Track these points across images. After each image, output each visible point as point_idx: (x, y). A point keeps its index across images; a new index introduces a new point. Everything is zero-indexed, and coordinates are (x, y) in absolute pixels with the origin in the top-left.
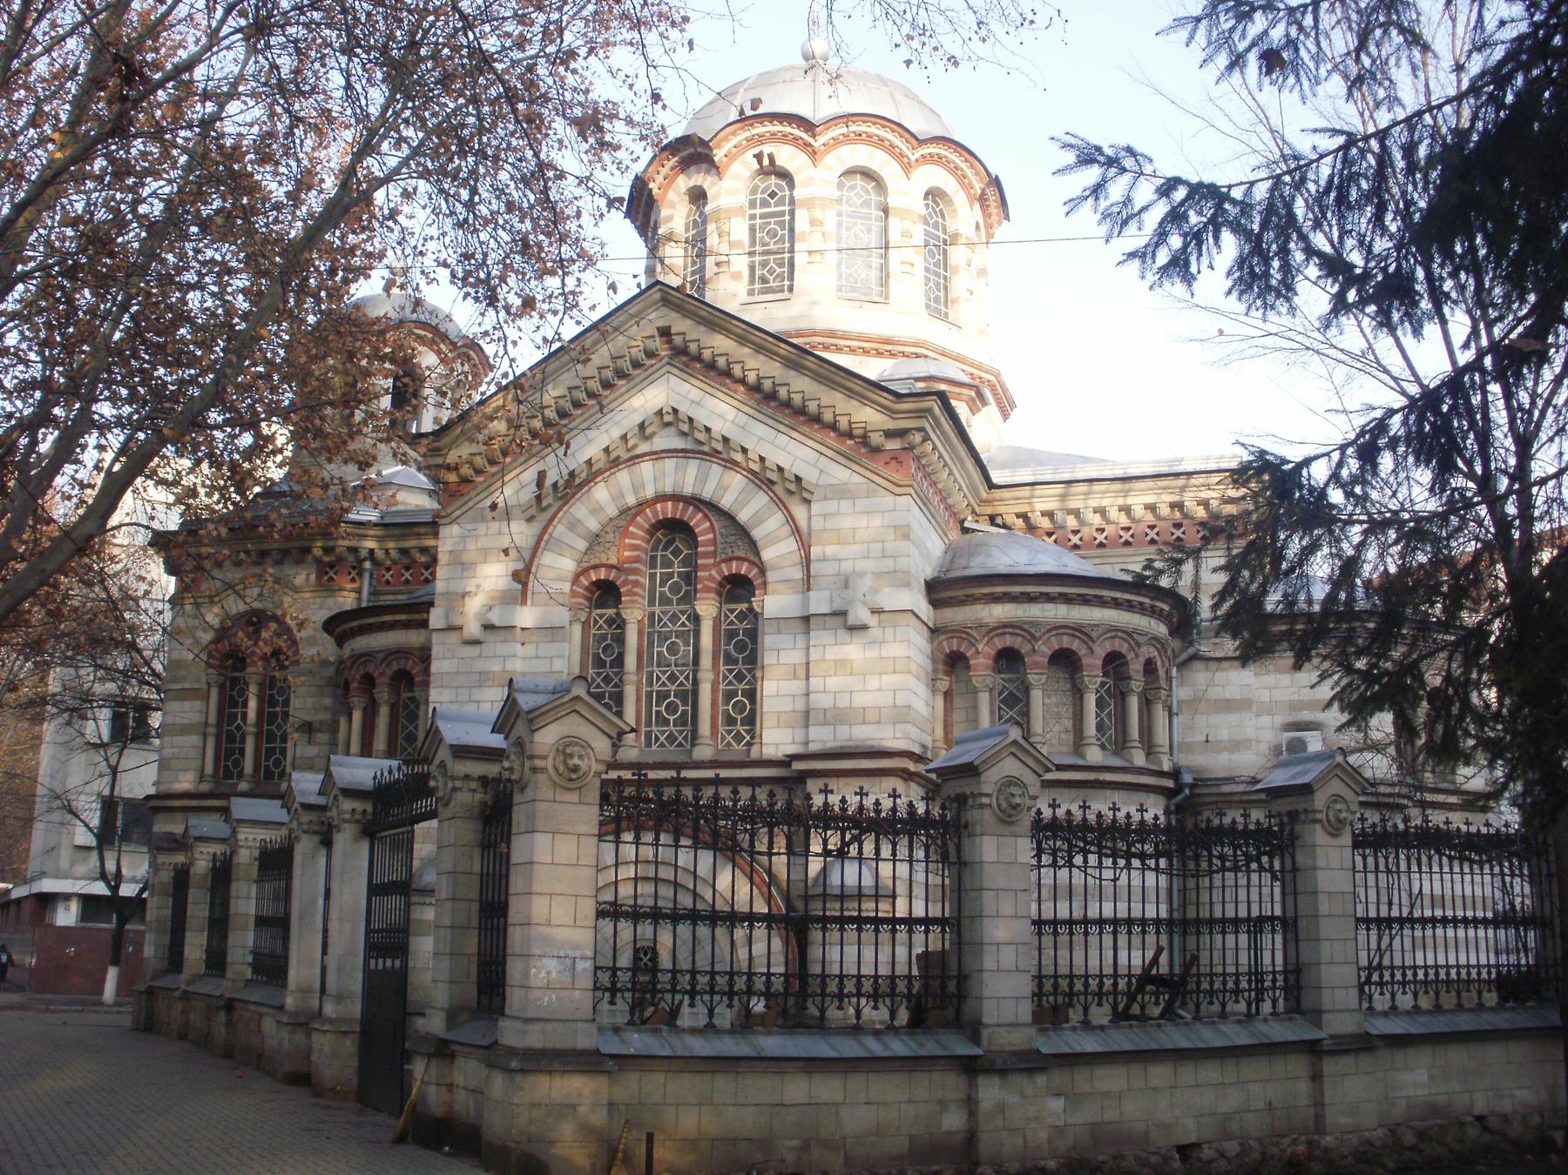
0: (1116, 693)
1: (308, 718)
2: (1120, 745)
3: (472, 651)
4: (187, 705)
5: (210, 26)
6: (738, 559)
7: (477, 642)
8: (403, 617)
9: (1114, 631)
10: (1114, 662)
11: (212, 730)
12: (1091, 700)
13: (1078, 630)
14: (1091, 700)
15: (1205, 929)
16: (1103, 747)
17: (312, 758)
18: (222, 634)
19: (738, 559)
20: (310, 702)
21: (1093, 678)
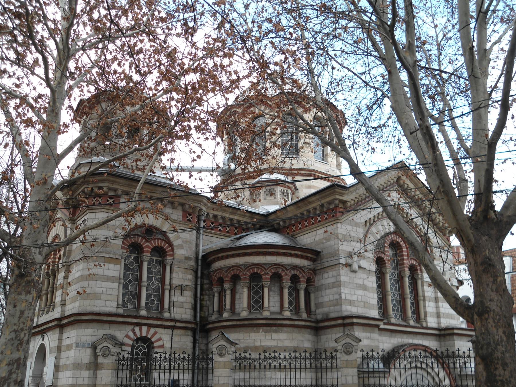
0: (294, 291)
1: (181, 283)
2: (297, 310)
3: (353, 275)
4: (111, 266)
5: (375, 57)
6: (158, 239)
7: (355, 272)
8: (299, 253)
9: (295, 267)
10: (295, 279)
11: (167, 287)
12: (286, 292)
13: (259, 265)
14: (286, 292)
16: (291, 311)
17: (182, 303)
19: (158, 239)
20: (181, 276)
21: (287, 283)
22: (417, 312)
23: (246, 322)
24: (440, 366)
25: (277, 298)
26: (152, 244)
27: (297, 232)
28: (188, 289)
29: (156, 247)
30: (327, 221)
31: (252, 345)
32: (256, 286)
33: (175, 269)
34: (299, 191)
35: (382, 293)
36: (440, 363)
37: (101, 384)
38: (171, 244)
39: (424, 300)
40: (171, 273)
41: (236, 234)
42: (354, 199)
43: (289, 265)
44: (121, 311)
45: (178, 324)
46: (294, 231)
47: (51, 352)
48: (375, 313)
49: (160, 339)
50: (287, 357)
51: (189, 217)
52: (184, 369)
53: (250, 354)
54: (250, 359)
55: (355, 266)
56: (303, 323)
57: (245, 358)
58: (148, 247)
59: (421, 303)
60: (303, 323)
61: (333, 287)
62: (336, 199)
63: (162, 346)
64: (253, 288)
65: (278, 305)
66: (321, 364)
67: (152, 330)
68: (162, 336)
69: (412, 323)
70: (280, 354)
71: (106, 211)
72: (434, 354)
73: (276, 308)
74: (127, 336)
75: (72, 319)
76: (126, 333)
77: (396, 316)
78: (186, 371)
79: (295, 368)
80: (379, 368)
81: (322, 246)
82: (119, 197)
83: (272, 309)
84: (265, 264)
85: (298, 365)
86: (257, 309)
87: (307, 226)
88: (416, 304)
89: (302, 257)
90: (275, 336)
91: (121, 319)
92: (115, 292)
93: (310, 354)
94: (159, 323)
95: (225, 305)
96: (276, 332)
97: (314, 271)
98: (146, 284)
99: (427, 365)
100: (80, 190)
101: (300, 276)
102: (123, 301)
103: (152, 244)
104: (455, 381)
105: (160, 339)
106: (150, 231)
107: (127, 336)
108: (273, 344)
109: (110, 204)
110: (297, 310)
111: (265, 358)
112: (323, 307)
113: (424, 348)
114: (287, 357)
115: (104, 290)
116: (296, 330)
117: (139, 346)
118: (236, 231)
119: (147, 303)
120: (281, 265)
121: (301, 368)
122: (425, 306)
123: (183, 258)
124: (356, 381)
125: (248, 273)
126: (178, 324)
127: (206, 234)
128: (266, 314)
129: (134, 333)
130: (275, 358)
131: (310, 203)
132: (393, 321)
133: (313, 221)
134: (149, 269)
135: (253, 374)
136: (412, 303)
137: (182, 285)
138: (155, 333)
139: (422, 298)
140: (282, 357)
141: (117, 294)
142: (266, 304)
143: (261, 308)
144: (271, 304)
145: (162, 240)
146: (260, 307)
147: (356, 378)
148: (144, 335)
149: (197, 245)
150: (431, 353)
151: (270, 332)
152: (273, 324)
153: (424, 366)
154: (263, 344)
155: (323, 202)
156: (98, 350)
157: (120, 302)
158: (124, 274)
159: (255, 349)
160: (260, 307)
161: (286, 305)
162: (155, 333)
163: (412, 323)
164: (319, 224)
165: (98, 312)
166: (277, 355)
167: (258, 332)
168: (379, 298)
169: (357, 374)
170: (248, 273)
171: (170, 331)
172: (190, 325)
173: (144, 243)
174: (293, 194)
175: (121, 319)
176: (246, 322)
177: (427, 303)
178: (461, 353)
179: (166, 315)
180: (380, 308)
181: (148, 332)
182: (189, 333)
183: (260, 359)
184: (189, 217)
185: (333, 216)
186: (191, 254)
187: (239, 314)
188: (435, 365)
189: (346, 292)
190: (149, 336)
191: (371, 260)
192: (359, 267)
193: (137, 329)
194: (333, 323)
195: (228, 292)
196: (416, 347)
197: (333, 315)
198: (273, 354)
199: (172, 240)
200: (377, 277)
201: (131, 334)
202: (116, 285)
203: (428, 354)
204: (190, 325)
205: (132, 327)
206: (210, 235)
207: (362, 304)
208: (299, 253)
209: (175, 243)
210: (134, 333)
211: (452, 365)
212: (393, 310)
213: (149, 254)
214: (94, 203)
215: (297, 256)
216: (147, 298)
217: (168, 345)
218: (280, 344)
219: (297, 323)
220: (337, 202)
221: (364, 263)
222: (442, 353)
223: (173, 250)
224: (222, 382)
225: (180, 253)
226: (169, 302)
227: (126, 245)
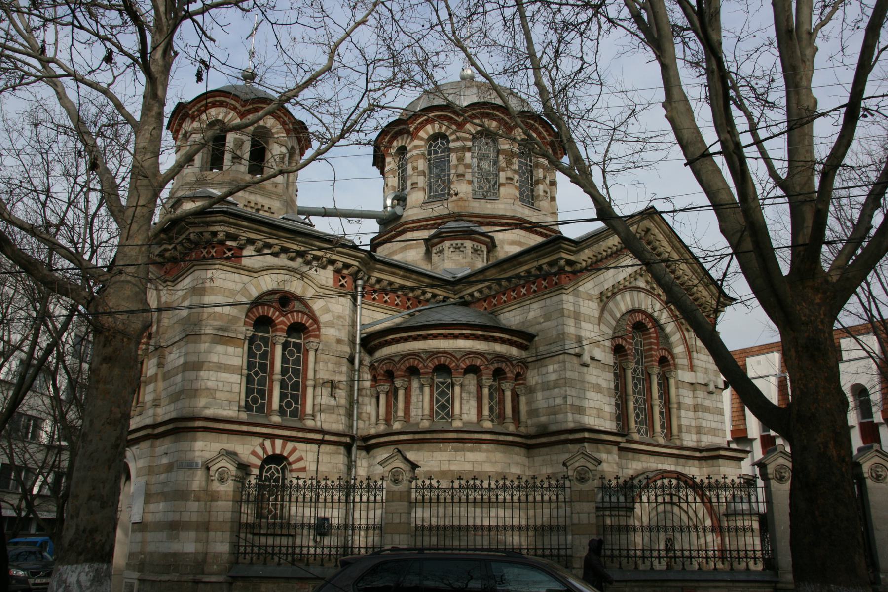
1: (331, 378)
6: (298, 312)
9: (499, 357)
13: (414, 354)
15: (741, 533)
18: (257, 302)
19: (298, 312)
22: (667, 426)
23: (428, 436)
24: (698, 500)
25: (474, 403)
26: (288, 319)
27: (499, 307)
28: (341, 386)
29: (295, 323)
30: (547, 291)
31: (436, 469)
32: (443, 383)
33: (321, 356)
34: (499, 248)
35: (620, 396)
36: (699, 495)
37: (216, 522)
38: (315, 320)
39: (679, 409)
40: (315, 362)
41: (408, 308)
42: (586, 259)
43: (490, 354)
44: (244, 416)
45: (327, 437)
46: (495, 305)
47: (138, 476)
48: (609, 425)
49: (300, 459)
50: (493, 486)
51: (343, 282)
52: (297, 501)
53: (438, 482)
54: (438, 488)
55: (586, 358)
56: (510, 438)
57: (431, 487)
58: (283, 322)
59: (674, 411)
60: (510, 438)
61: (554, 388)
62: (562, 258)
63: (304, 469)
64: (438, 387)
65: (474, 411)
66: (542, 496)
67: (290, 445)
68: (304, 455)
69: (661, 440)
70: (482, 482)
71: (220, 267)
72: (690, 482)
73: (474, 418)
74: (254, 453)
75: (170, 426)
76: (251, 449)
77: (639, 431)
78: (539, 505)
79: (460, 502)
80: (618, 502)
81: (538, 327)
82: (241, 248)
83: (465, 417)
84: (456, 352)
85: (464, 498)
86: (443, 418)
87: (515, 298)
88: (667, 414)
89: (511, 343)
90: (470, 456)
91: (244, 428)
92: (236, 388)
93: (512, 481)
94: (300, 434)
95: (396, 412)
96: (471, 450)
97: (524, 364)
98: (280, 377)
99: (680, 498)
100: (183, 236)
101: (507, 370)
102: (247, 401)
103: (288, 319)
104: (719, 521)
105: (300, 459)
106: (285, 299)
107: (254, 453)
108: (468, 467)
109: (228, 258)
110: (501, 417)
111: (461, 487)
112: (538, 416)
113: (675, 475)
114: (493, 486)
115: (220, 385)
116: (501, 447)
117: (271, 468)
118: (409, 304)
119: (281, 406)
120: (445, 352)
121: (453, 502)
122: (679, 417)
123: (335, 340)
124: (593, 520)
125: (430, 364)
126: (327, 437)
127: (366, 307)
128: (457, 424)
129: (264, 449)
130: (475, 488)
131: (521, 264)
132: (636, 437)
133: (524, 291)
134: (283, 355)
135: (539, 511)
136: (661, 413)
137: (332, 382)
138: (294, 450)
139: (675, 406)
140: (486, 485)
141: (238, 391)
142: (457, 410)
143: (451, 416)
144: (464, 411)
145: (304, 313)
146: (447, 415)
147: (593, 516)
148: (278, 452)
149: (353, 324)
150: (685, 482)
151: (463, 450)
152: (464, 438)
153: (675, 499)
154: (452, 468)
155: (541, 262)
156: (212, 473)
157: (243, 403)
158: (249, 362)
159: (443, 474)
160: (447, 415)
161: (486, 412)
162: (294, 450)
163: (661, 440)
164: (533, 295)
165: (211, 417)
166: (478, 482)
167: (445, 451)
168: (617, 405)
169: (594, 510)
170: (430, 364)
171: (315, 447)
172: (343, 439)
173: (278, 317)
174: (489, 252)
175: (244, 428)
176: (428, 436)
177: (683, 413)
178: (728, 481)
179: (310, 423)
180: (618, 418)
181: (284, 447)
182: (342, 450)
183: (453, 488)
184: (343, 282)
185: (556, 283)
186: (344, 336)
187: (418, 424)
188: (690, 499)
189: (574, 394)
190: (285, 454)
191: (607, 349)
192: (592, 358)
193: (268, 443)
194: (553, 439)
195: (401, 393)
196: (664, 474)
197: (553, 428)
198: (427, 482)
199: (317, 313)
200: (616, 375)
201: (260, 451)
202: (236, 378)
203: (682, 484)
204: (343, 439)
205: (261, 440)
206: (371, 308)
207: (595, 412)
208: (506, 336)
209: (323, 318)
210: (264, 449)
211: (714, 500)
212: (636, 422)
213: (284, 334)
214: (204, 257)
215: (503, 341)
216: (281, 400)
217: (312, 467)
218: (477, 468)
219: (501, 438)
220: (562, 262)
221: (598, 354)
222: (701, 481)
223: (319, 329)
224: (398, 521)
225: (329, 333)
226: (314, 405)
227: (251, 319)
